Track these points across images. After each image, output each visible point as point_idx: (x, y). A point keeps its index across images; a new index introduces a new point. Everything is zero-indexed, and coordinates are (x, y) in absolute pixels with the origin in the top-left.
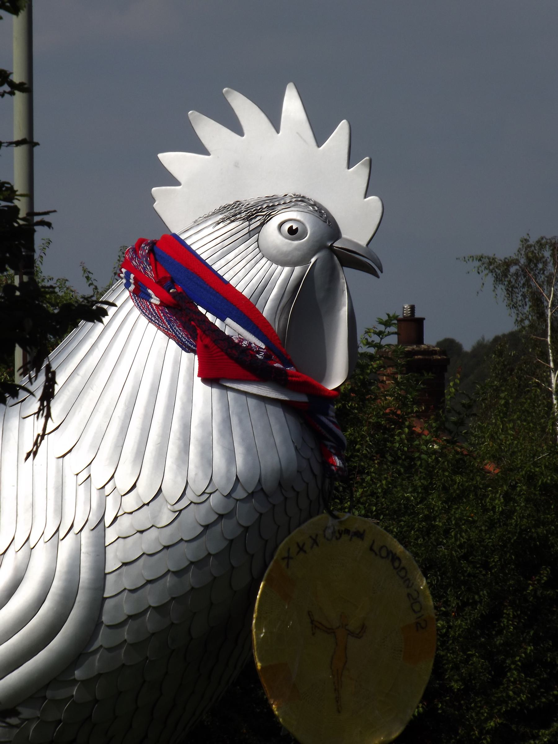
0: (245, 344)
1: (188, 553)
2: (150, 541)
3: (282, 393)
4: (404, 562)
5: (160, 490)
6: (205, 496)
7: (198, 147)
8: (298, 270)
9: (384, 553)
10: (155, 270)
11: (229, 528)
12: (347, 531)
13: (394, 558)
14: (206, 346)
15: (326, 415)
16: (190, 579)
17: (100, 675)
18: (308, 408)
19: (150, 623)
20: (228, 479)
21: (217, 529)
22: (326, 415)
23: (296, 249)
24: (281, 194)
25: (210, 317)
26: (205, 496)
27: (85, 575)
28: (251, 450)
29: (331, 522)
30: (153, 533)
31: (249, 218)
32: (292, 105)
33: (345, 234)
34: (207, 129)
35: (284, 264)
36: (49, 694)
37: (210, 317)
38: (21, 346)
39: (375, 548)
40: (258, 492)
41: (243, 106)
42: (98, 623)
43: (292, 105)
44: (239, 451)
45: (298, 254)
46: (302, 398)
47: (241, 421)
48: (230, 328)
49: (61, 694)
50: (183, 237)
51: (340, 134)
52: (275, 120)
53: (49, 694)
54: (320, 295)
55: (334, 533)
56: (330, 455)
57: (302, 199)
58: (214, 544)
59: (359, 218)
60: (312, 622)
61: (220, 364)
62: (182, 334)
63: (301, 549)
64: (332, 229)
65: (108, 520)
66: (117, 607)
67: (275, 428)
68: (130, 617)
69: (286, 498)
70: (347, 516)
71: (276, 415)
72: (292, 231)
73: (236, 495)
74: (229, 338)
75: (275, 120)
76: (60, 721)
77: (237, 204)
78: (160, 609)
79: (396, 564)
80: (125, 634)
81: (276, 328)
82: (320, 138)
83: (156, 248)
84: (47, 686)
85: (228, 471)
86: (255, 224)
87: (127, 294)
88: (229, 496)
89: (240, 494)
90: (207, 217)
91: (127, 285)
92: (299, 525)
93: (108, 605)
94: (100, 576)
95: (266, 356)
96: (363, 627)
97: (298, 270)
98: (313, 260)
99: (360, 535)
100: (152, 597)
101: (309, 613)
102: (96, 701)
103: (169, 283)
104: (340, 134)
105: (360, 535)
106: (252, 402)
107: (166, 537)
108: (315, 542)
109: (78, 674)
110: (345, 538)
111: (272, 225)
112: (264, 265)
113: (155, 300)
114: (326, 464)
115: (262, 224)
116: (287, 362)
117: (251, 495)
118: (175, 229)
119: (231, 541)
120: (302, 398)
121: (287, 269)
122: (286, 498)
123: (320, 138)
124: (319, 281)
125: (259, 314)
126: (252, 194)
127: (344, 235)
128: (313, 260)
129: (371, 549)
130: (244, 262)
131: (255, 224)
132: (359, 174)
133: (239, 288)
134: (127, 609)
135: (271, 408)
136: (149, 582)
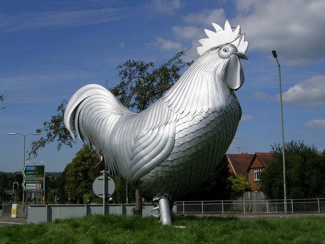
1: (197, 127)
2: (187, 125)
21: (204, 121)
28: (213, 102)
32: (215, 25)
44: (210, 102)
64: (235, 49)
72: (226, 50)
107: (191, 123)
109: (169, 159)
134: (181, 143)
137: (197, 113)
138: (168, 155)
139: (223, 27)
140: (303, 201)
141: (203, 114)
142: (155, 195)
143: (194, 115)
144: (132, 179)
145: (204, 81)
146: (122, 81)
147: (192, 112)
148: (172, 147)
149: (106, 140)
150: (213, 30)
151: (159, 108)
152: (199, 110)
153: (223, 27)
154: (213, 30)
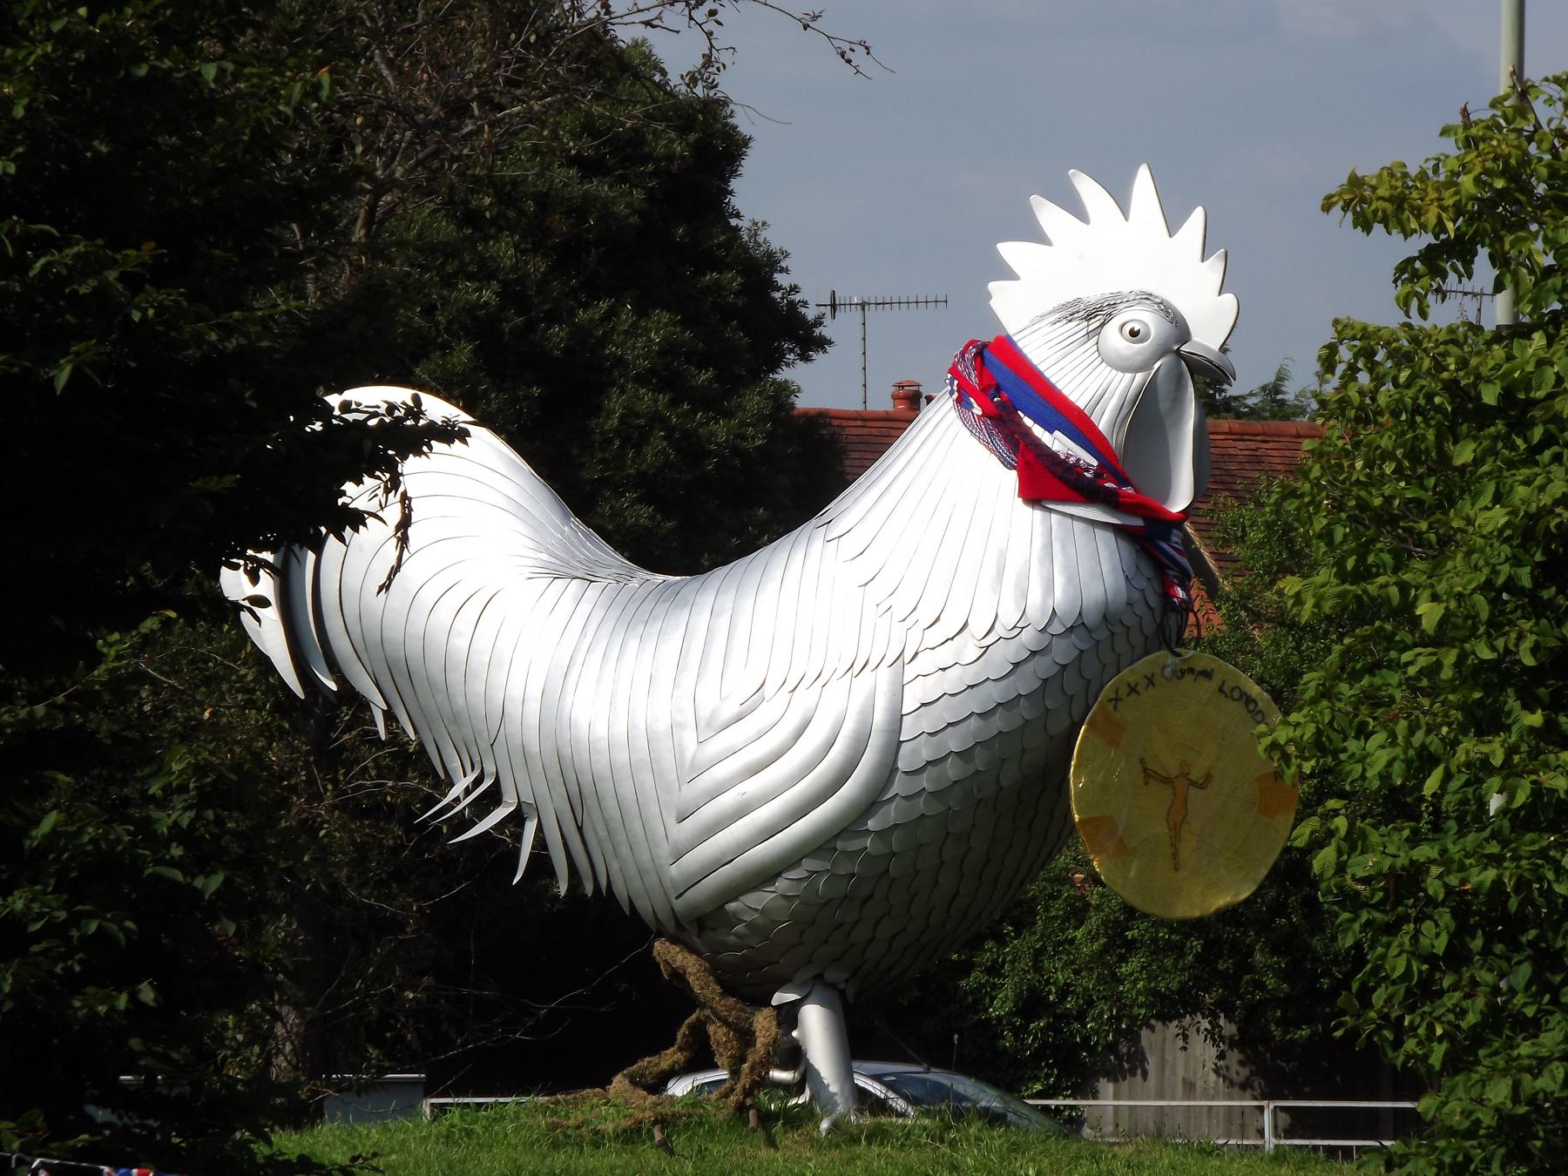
0: (1072, 460)
1: (995, 694)
2: (953, 680)
3: (1113, 516)
4: (1261, 705)
5: (966, 625)
6: (1017, 631)
7: (1040, 237)
8: (1139, 377)
9: (1236, 695)
10: (980, 376)
11: (1044, 667)
12: (1191, 670)
13: (1249, 700)
14: (1027, 463)
15: (1167, 540)
16: (998, 724)
17: (896, 826)
18: (1147, 534)
19: (952, 771)
20: (1043, 613)
21: (1030, 666)
22: (1167, 540)
23: (1138, 353)
24: (1126, 290)
25: (1038, 431)
26: (1017, 631)
27: (880, 717)
28: (1072, 579)
29: (1170, 659)
30: (956, 670)
31: (1088, 318)
32: (1143, 185)
33: (1196, 337)
34: (1049, 215)
35: (1124, 370)
36: (839, 845)
37: (1038, 431)
38: (54, 390)
39: (1226, 689)
40: (1078, 627)
41: (1088, 189)
42: (894, 769)
43: (1143, 185)
44: (1059, 581)
45: (1139, 359)
46: (1139, 522)
47: (1064, 547)
48: (1058, 443)
49: (853, 845)
50: (1015, 339)
51: (1195, 221)
52: (1124, 206)
53: (839, 845)
54: (1164, 406)
55: (1174, 672)
56: (1172, 585)
57: (1148, 297)
58: (1025, 684)
59: (1210, 321)
60: (1145, 770)
61: (1044, 482)
62: (1003, 449)
63: (1133, 689)
64: (1181, 331)
65: (908, 655)
66: (915, 752)
67: (1104, 555)
68: (929, 763)
69: (1113, 634)
70: (1191, 653)
71: (1106, 540)
72: (1134, 333)
73: (1052, 630)
74: (1054, 455)
75: (1124, 206)
76: (853, 875)
77: (1079, 301)
78: (964, 755)
79: (1251, 707)
80: (924, 782)
81: (1113, 443)
82: (1172, 227)
83: (987, 353)
84: (837, 836)
85: (1044, 603)
86: (1095, 324)
87: (950, 403)
88: (1043, 630)
89: (1057, 628)
90: (1043, 317)
91: (951, 393)
92: (1132, 662)
93: (904, 749)
94: (897, 719)
95: (1098, 474)
96: (1209, 777)
97: (1139, 377)
98: (1157, 366)
99: (1207, 674)
100: (954, 742)
101: (1142, 761)
102: (893, 854)
103: (992, 391)
104: (1195, 221)
105: (1207, 674)
106: (1078, 526)
107: (971, 676)
108: (1151, 681)
109: (871, 824)
110: (1189, 677)
111: (1112, 329)
112: (1105, 370)
113: (978, 411)
114: (1167, 596)
115: (1103, 325)
116: (1123, 480)
117: (1071, 629)
118: (1011, 331)
119: (1046, 680)
120: (1139, 522)
121: (1128, 376)
122: (1113, 634)
123: (1172, 227)
124: (1163, 389)
125: (1093, 428)
126: (1092, 292)
127: (1195, 338)
128: (1157, 366)
129: (1221, 690)
130: (1090, 369)
131: (1095, 324)
132: (1213, 270)
133: (1072, 398)
134: (926, 755)
135: (1100, 533)
136: (950, 724)
137: (1000, 630)
138: (871, 802)
139: (1123, 203)
140: (468, 792)
141: (1028, 636)
142: (780, 983)
143: (986, 642)
144: (678, 904)
145: (887, 497)
146: (401, 489)
147: (979, 626)
148: (888, 770)
149: (513, 710)
150: (1077, 209)
151: (723, 622)
152: (1009, 617)
153: (1123, 203)
154: (1077, 209)
